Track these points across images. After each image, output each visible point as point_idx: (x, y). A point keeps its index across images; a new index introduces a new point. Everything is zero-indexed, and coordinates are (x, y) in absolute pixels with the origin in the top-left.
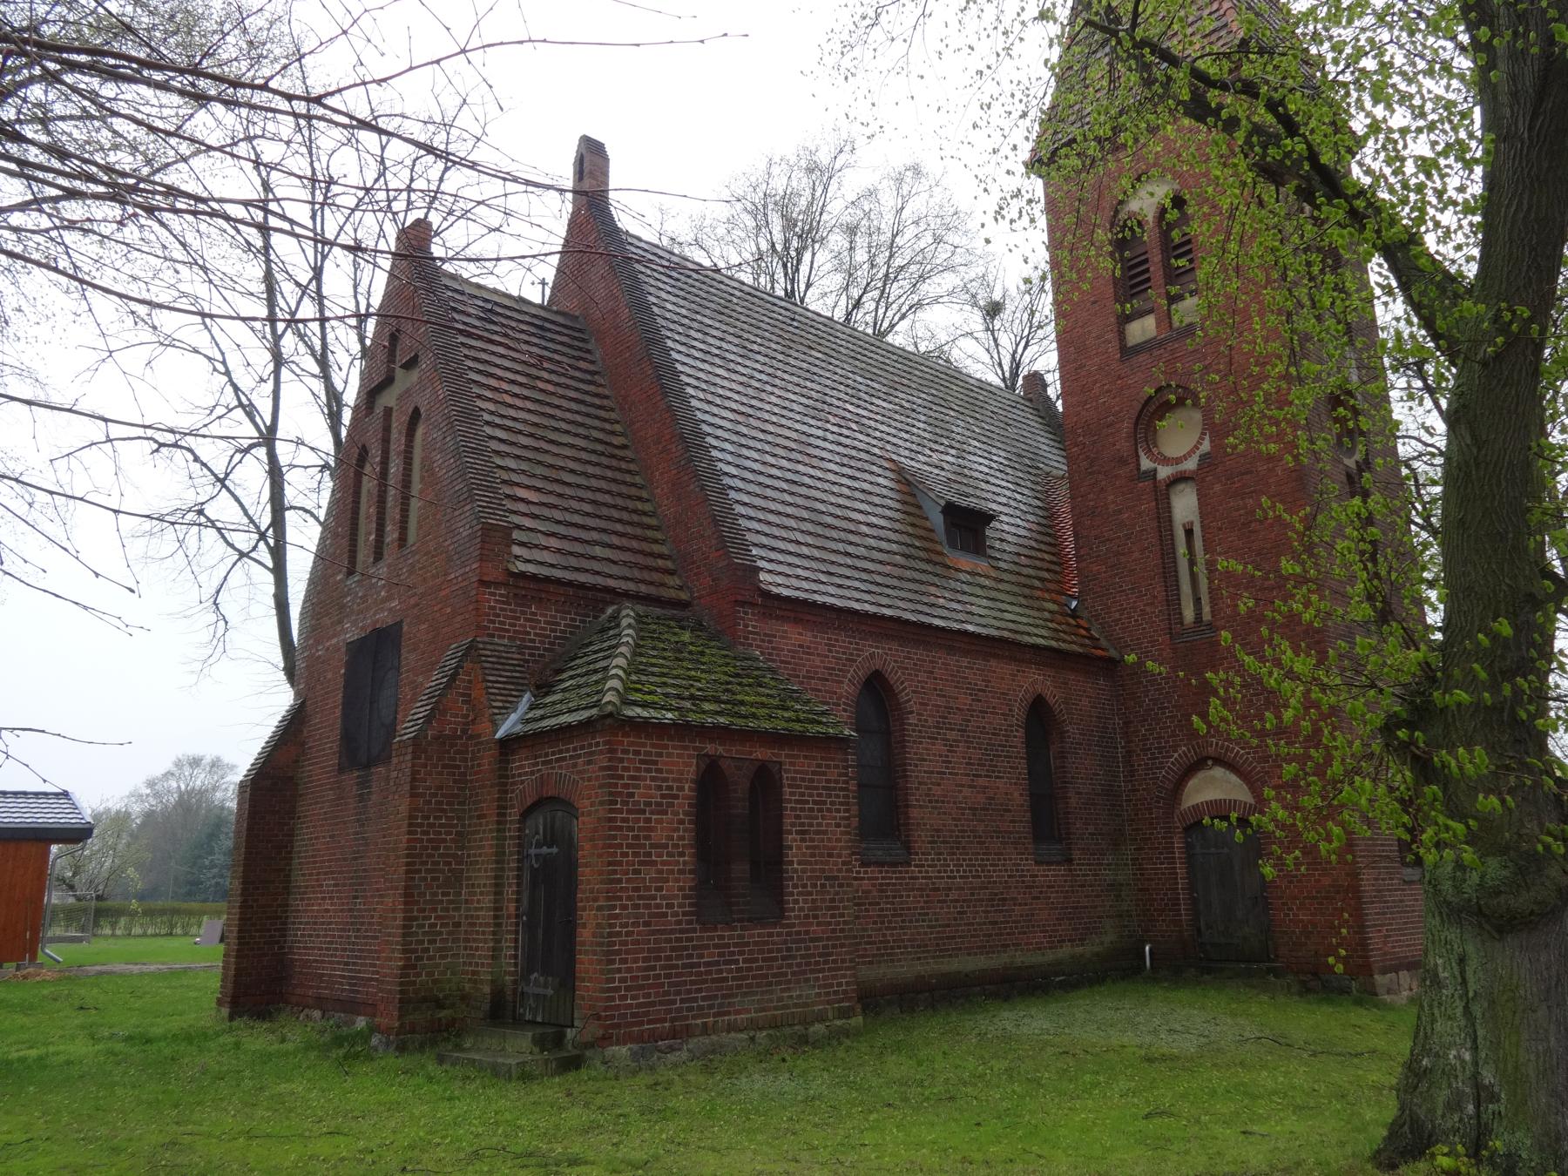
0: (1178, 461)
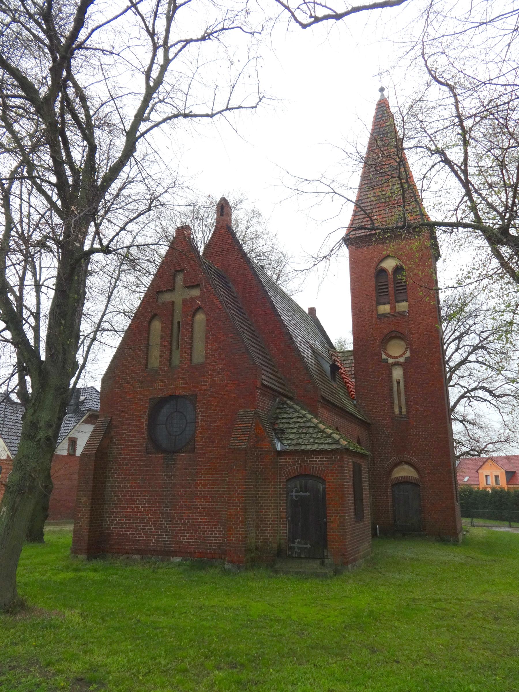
0: (396, 357)
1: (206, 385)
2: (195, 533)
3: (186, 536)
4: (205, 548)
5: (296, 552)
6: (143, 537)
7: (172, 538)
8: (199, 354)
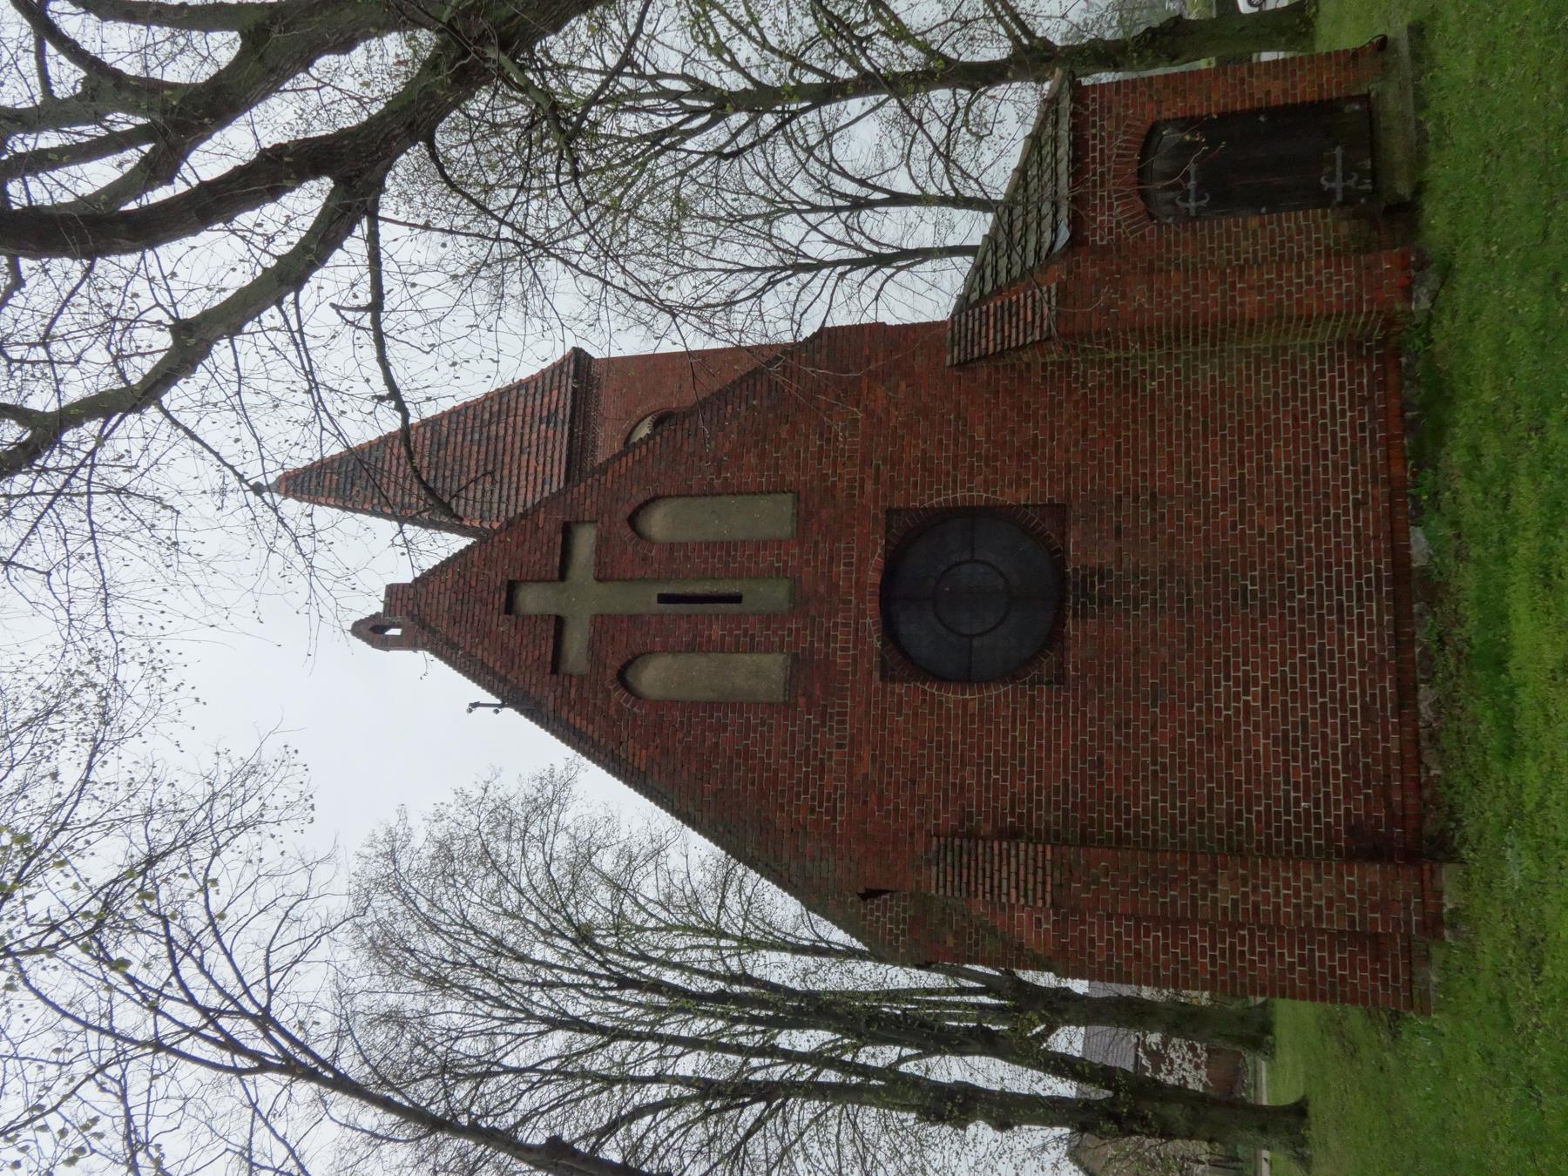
1: (862, 480)
2: (1326, 482)
3: (1337, 516)
4: (1373, 446)
5: (1359, 183)
6: (1352, 684)
7: (1348, 566)
8: (770, 517)
